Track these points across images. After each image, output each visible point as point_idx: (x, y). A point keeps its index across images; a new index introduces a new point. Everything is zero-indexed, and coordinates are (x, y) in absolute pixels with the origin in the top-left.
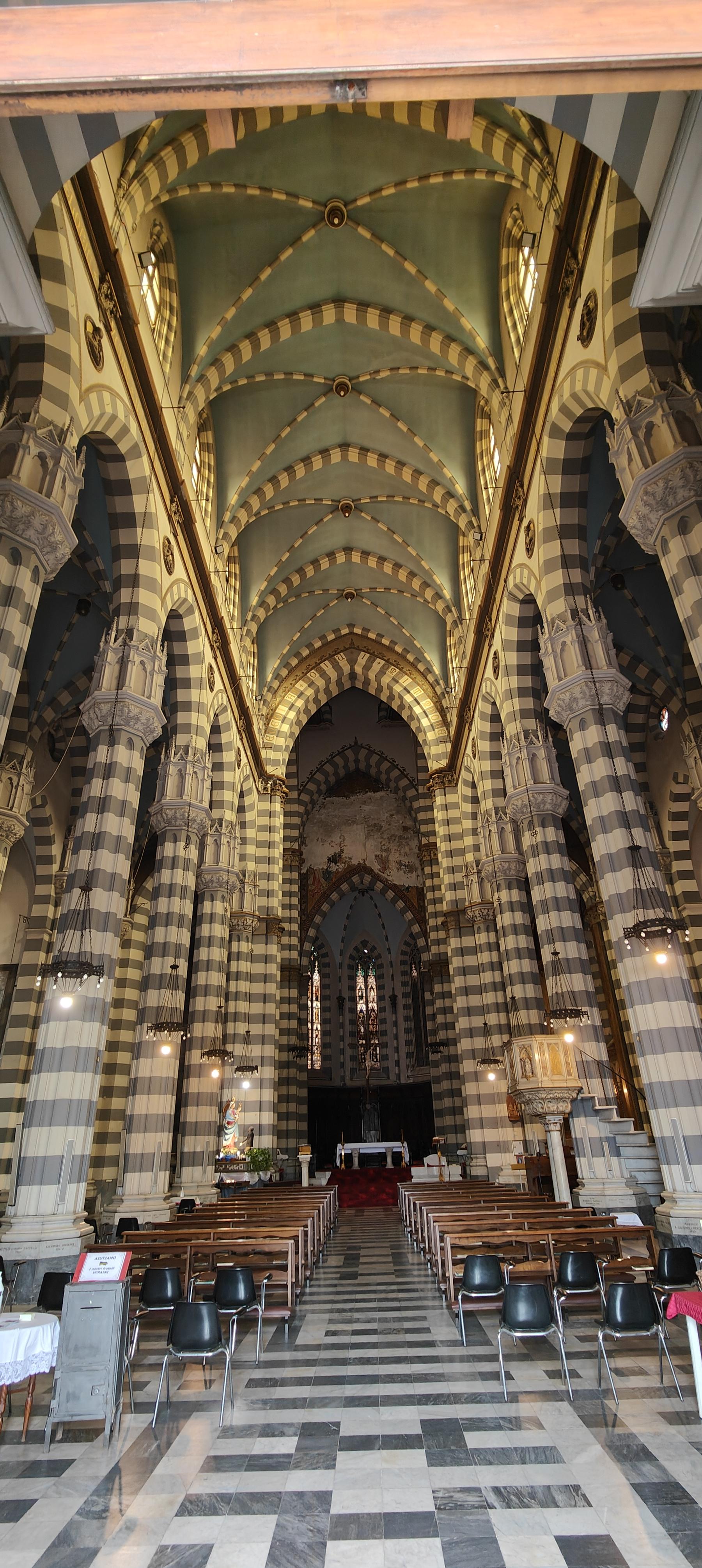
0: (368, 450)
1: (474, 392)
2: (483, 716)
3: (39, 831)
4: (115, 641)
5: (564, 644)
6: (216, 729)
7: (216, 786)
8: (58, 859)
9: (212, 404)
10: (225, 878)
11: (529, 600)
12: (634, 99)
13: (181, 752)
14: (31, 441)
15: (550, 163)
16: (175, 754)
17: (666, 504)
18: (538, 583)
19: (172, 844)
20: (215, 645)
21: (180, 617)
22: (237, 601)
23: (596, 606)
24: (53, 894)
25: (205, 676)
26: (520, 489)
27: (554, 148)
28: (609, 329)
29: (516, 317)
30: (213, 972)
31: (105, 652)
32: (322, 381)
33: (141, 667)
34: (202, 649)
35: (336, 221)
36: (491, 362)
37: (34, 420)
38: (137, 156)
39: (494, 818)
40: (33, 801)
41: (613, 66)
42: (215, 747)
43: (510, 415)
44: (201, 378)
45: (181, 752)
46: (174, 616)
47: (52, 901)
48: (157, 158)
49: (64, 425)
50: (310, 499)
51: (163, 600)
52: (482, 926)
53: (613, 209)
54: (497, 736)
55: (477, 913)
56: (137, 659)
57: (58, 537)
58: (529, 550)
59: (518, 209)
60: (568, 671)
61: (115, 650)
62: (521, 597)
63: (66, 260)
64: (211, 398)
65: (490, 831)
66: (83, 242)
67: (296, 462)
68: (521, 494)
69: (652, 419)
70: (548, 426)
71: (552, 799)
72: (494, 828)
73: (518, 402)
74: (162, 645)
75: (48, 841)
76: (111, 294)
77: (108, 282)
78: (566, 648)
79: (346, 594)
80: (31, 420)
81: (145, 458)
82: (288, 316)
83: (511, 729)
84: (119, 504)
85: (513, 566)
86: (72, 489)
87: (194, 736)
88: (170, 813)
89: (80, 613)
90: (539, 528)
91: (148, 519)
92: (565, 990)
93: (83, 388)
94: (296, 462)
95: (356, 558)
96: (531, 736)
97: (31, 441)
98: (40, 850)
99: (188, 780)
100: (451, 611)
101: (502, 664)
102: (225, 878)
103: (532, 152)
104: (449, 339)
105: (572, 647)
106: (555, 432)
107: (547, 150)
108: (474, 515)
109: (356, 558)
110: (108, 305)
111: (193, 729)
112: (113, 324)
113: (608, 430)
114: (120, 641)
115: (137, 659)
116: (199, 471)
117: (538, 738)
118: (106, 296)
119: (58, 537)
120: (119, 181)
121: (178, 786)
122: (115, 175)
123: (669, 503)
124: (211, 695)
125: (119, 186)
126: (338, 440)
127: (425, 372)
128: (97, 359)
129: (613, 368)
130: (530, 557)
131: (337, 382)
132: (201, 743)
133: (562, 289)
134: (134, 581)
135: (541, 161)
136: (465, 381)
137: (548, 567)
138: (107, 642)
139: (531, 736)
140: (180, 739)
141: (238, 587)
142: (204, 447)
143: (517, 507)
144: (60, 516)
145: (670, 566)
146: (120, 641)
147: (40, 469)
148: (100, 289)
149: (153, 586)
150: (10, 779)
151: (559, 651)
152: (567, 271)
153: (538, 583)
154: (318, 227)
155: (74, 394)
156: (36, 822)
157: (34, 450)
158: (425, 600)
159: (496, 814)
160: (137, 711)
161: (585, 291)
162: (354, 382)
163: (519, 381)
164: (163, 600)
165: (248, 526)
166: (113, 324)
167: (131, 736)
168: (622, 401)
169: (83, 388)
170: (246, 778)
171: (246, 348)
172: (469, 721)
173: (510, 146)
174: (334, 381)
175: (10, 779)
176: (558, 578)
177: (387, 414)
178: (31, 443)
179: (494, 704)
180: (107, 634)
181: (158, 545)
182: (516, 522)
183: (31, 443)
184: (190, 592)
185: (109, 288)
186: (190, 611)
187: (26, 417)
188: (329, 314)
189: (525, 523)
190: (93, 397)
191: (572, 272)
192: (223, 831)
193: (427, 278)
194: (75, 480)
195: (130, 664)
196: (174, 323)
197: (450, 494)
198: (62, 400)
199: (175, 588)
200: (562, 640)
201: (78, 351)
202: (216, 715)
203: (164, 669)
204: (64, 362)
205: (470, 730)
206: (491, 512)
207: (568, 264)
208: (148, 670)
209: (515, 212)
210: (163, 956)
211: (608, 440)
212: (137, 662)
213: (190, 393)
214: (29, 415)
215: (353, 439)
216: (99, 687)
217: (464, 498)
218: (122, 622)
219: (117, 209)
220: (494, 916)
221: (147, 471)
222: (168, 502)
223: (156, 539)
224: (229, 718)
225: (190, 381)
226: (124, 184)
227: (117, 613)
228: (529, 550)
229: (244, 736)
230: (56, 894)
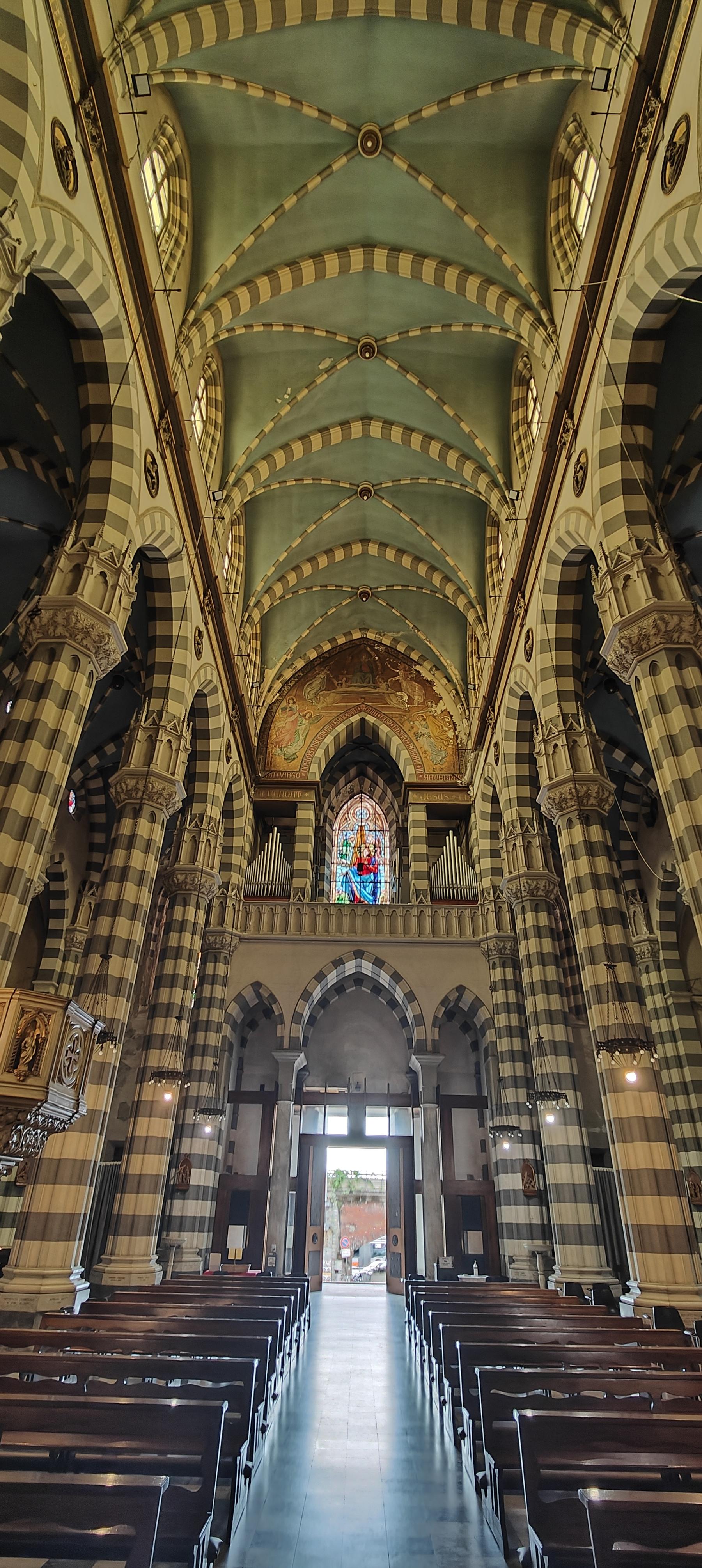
0: (392, 424)
1: (484, 506)
2: (509, 713)
3: (54, 886)
4: (146, 720)
5: (556, 746)
6: (229, 797)
7: (228, 850)
8: (70, 914)
9: (246, 506)
10: (229, 940)
11: (526, 698)
12: (510, 694)
13: (197, 819)
14: (95, 562)
15: (554, 332)
16: (191, 822)
17: (641, 648)
18: (535, 687)
19: (182, 908)
20: (234, 720)
21: (205, 696)
22: (239, 583)
23: (585, 714)
24: (62, 948)
25: (224, 749)
26: (569, 421)
27: (558, 321)
28: (596, 490)
29: (524, 447)
30: (212, 1033)
31: (135, 729)
32: (346, 340)
33: (167, 745)
34: (222, 725)
35: (367, 355)
36: (500, 479)
37: (97, 545)
38: (196, 307)
39: (519, 830)
40: (52, 858)
41: (340, 1292)
42: (228, 814)
43: (557, 351)
44: (210, 307)
45: (197, 819)
46: (200, 696)
47: (61, 955)
48: (167, 20)
49: (122, 547)
50: (331, 585)
51: (191, 683)
52: (497, 961)
53: (601, 390)
54: (496, 817)
55: (491, 946)
56: (165, 738)
57: (112, 646)
58: (528, 655)
59: (527, 357)
60: (559, 772)
61: (69, 556)
62: (521, 693)
63: (135, 408)
64: (245, 501)
65: (515, 845)
66: (153, 406)
67: (304, 257)
68: (522, 604)
69: (630, 573)
70: (611, 324)
71: (598, 793)
72: (519, 842)
73: (522, 526)
74: (188, 725)
75: (61, 895)
76: (169, 427)
77: (91, 100)
78: (557, 750)
79: (361, 491)
80: (95, 544)
81: (185, 559)
82: (320, 431)
83: (509, 815)
84: (92, 394)
85: (514, 665)
86: (126, 602)
87: (209, 806)
88: (181, 878)
89: (114, 687)
90: (537, 638)
91: (128, 419)
92: (549, 1071)
93: (140, 513)
94: (304, 257)
95: (376, 429)
96: (571, 720)
97: (95, 562)
98: (54, 904)
99: (202, 847)
100: (473, 607)
101: (501, 752)
102: (229, 940)
103: (539, 320)
104: (465, 457)
105: (639, 581)
106: (552, 558)
107: (552, 321)
108: (544, 308)
109: (376, 429)
110: (164, 436)
111: (209, 799)
112: (168, 453)
113: (594, 573)
114: (150, 720)
115: (165, 738)
116: (230, 561)
117: (533, 826)
118: (164, 430)
119: (112, 646)
120: (180, 328)
121: (191, 853)
122: (178, 322)
123: (644, 647)
124: (197, 664)
125: (180, 332)
126: (358, 413)
127: (460, 329)
128: (153, 486)
129: (599, 521)
130: (578, 495)
131: (362, 132)
132: (214, 812)
133: (560, 441)
134: (167, 668)
135: (546, 329)
136: (477, 495)
137: (543, 674)
138: (137, 720)
139: (571, 720)
140: (197, 808)
141: (241, 569)
142: (237, 539)
143: (519, 615)
144: (116, 630)
145: (643, 699)
146: (150, 720)
147: (101, 586)
148: (159, 425)
149: (183, 670)
150: (90, 903)
151: (551, 753)
152: (564, 428)
153: (535, 687)
154: (351, 359)
155: (132, 520)
156: (54, 876)
157: (97, 570)
158: (445, 596)
159: (522, 826)
160: (160, 787)
161: (578, 447)
162: (376, 488)
163: (524, 508)
164: (191, 683)
165: (272, 608)
166: (168, 453)
167: (153, 809)
168: (604, 553)
169: (140, 513)
170: (236, 779)
171: (280, 458)
172: (492, 722)
173: (519, 312)
174: (359, 342)
175: (90, 903)
176: (551, 685)
177: (429, 186)
178: (95, 565)
179: (494, 787)
180: (139, 713)
181: (191, 636)
182: (517, 628)
183: (95, 565)
184: (215, 673)
185: (167, 422)
186: (214, 691)
187: (91, 541)
188: (357, 549)
189: (493, 742)
190: (147, 520)
191: (568, 430)
192: (229, 893)
193: (445, 404)
194: (130, 594)
195: (86, 572)
196: (218, 438)
197: (460, 591)
198: (122, 525)
199: (202, 671)
200: (625, 573)
201: (137, 481)
202: (230, 784)
203: (188, 746)
204: (126, 494)
205: (493, 733)
206: (498, 612)
207: (565, 423)
208: (174, 748)
209: (525, 359)
210: (166, 1017)
211: (593, 583)
212: (165, 741)
213: (196, 321)
214: (94, 538)
215: (373, 412)
216: (127, 762)
217: (496, 470)
218: (155, 704)
219: (178, 352)
220: (516, 942)
221: (187, 572)
222: (202, 597)
223: (189, 629)
224: (218, 700)
225: (228, 487)
226: (185, 331)
227: (149, 694)
228: (528, 655)
229: (236, 727)
230: (66, 946)
